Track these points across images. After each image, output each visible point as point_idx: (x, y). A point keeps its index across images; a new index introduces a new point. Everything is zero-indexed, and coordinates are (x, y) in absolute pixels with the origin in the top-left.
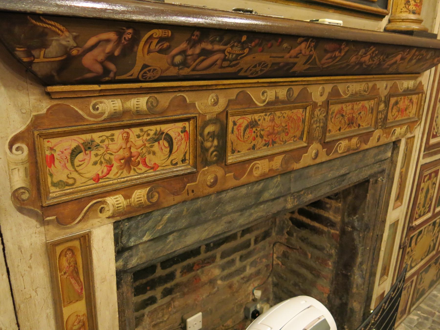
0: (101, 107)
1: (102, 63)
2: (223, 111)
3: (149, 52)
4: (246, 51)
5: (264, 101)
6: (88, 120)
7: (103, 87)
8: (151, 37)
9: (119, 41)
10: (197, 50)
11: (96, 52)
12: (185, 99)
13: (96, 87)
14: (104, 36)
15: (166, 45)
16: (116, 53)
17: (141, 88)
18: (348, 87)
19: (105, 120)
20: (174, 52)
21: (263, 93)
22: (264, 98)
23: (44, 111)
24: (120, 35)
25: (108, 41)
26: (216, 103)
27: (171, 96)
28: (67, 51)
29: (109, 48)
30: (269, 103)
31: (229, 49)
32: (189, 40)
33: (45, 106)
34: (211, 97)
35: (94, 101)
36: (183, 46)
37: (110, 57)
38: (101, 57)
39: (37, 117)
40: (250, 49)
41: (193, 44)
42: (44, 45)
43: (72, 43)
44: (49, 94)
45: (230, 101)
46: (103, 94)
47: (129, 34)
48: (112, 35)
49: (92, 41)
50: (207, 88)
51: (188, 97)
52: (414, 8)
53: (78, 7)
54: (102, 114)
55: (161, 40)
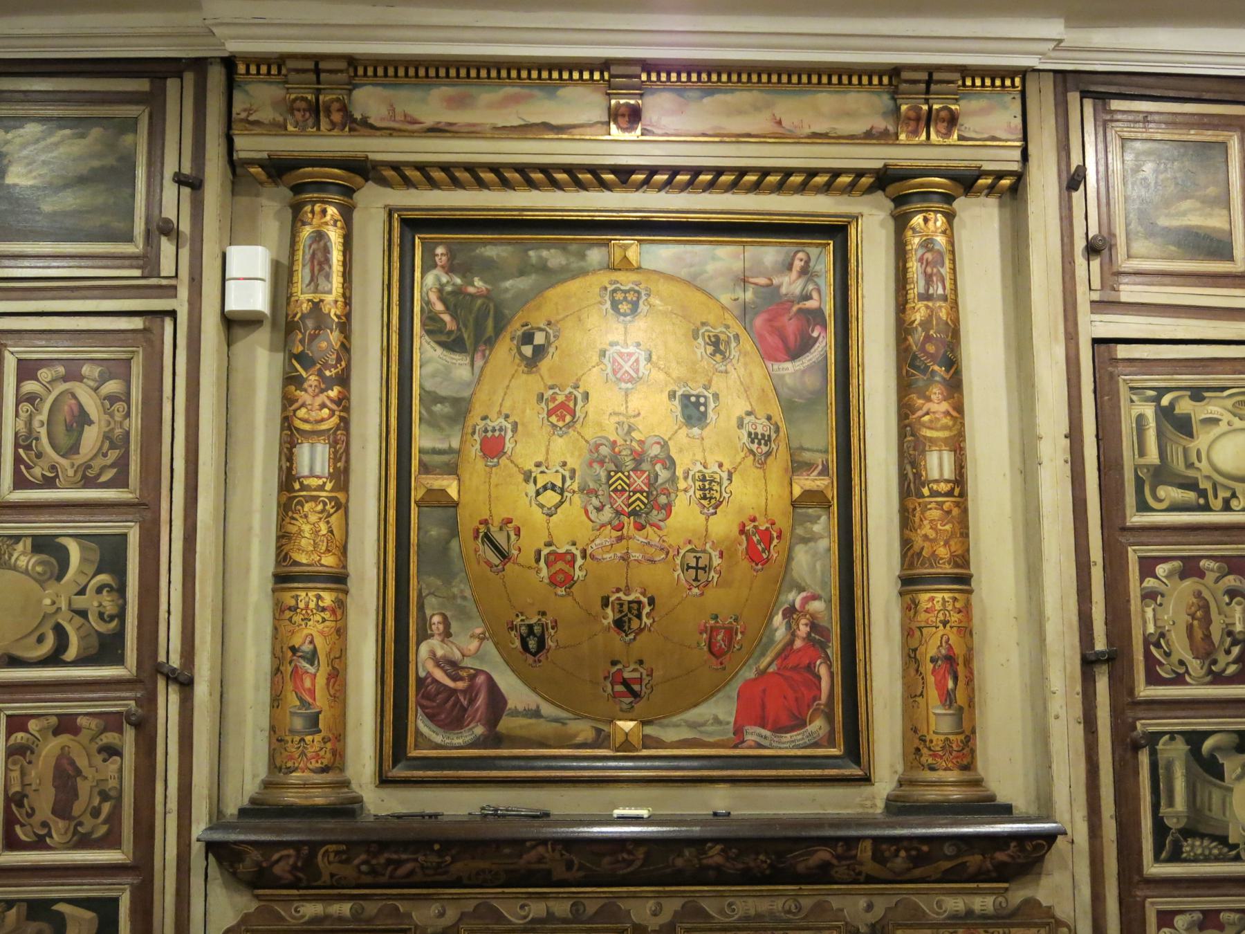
0: (302, 910)
1: (290, 872)
2: (453, 926)
3: (330, 863)
4: (448, 859)
5: (525, 917)
6: (510, 922)
7: (302, 892)
8: (327, 851)
9: (298, 856)
10: (382, 860)
11: (281, 864)
12: (397, 909)
13: (295, 892)
14: (285, 852)
15: (344, 857)
16: (299, 864)
17: (340, 895)
18: (730, 905)
19: (305, 923)
20: (356, 862)
21: (522, 907)
22: (523, 913)
23: (252, 910)
24: (298, 851)
25: (289, 856)
26: (870, 907)
27: (381, 904)
28: (258, 864)
29: (291, 861)
30: (533, 921)
31: (421, 858)
32: (368, 852)
33: (253, 906)
34: (434, 908)
35: (296, 904)
36: (363, 857)
37: (294, 867)
38: (287, 868)
39: (246, 914)
40: (453, 857)
41: (375, 855)
42: (241, 860)
43: (260, 858)
44: (257, 897)
45: (463, 915)
46: (304, 898)
47: (305, 850)
48: (291, 852)
49: (276, 856)
50: (427, 897)
51: (402, 907)
52: (930, 760)
53: (1119, 401)
54: (303, 917)
55: (337, 853)
